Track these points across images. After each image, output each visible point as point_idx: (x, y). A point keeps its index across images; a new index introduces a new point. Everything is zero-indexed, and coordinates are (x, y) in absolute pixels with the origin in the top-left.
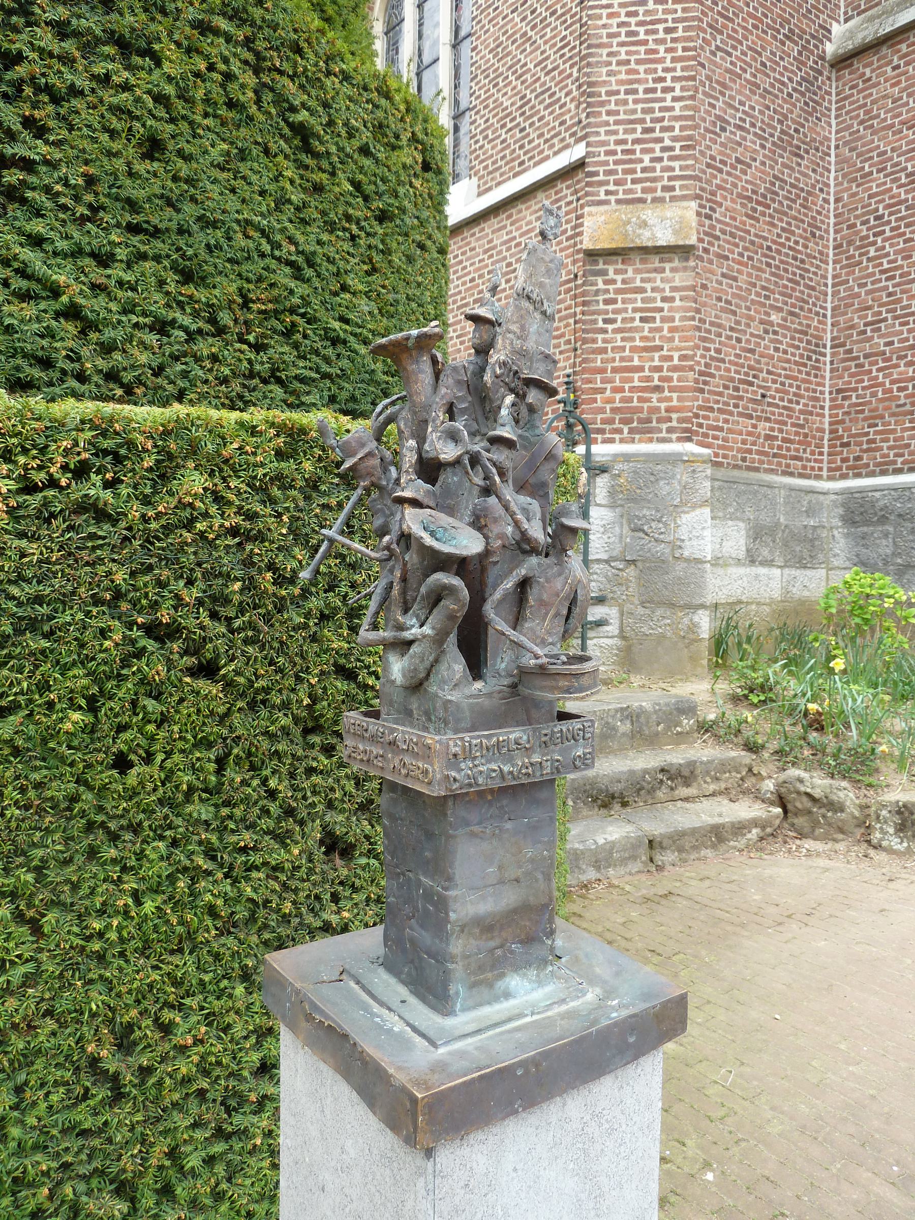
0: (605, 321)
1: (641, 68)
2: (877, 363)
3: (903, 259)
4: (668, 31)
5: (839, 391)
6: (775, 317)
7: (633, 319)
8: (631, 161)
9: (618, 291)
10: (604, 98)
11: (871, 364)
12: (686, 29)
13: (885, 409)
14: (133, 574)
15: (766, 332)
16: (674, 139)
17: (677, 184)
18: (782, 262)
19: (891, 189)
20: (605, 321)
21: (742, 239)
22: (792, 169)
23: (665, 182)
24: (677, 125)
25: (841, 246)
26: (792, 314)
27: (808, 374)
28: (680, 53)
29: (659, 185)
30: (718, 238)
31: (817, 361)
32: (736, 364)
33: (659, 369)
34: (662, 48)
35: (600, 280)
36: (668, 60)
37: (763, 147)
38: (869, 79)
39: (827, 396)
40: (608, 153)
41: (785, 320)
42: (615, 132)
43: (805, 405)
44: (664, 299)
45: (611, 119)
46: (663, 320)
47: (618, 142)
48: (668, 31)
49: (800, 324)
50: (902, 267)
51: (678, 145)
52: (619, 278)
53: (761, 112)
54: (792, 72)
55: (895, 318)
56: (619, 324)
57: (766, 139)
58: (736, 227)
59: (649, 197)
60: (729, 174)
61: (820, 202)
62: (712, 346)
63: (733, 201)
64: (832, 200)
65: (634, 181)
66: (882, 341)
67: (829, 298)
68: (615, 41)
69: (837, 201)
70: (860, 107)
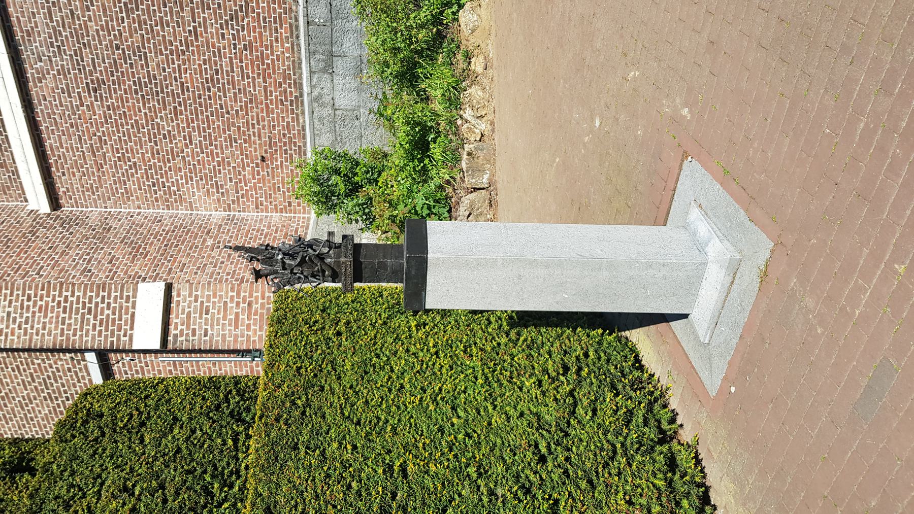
1: (50, 315)
4: (29, 299)
5: (257, 208)
6: (210, 242)
7: (206, 319)
8: (107, 322)
9: (188, 328)
10: (64, 338)
11: (242, 190)
12: (30, 289)
13: (269, 182)
16: (97, 296)
17: (125, 294)
18: (175, 239)
20: (206, 335)
22: (117, 233)
23: (123, 301)
24: (89, 294)
26: (208, 233)
27: (245, 225)
28: (44, 292)
29: (125, 304)
30: (158, 274)
31: (238, 219)
32: (237, 264)
33: (238, 304)
34: (39, 303)
35: (179, 339)
36: (47, 299)
37: (102, 249)
38: (67, 189)
40: (100, 336)
42: (88, 331)
43: (264, 226)
44: (196, 301)
45: (79, 333)
47: (94, 329)
48: (29, 299)
51: (101, 293)
52: (180, 327)
53: (80, 250)
54: (56, 232)
55: (216, 176)
56: (209, 327)
57: (98, 247)
59: (131, 310)
60: (118, 268)
63: (135, 265)
64: (138, 210)
65: (120, 319)
66: (229, 183)
67: (199, 212)
68: (29, 331)
69: (139, 208)
70: (84, 194)
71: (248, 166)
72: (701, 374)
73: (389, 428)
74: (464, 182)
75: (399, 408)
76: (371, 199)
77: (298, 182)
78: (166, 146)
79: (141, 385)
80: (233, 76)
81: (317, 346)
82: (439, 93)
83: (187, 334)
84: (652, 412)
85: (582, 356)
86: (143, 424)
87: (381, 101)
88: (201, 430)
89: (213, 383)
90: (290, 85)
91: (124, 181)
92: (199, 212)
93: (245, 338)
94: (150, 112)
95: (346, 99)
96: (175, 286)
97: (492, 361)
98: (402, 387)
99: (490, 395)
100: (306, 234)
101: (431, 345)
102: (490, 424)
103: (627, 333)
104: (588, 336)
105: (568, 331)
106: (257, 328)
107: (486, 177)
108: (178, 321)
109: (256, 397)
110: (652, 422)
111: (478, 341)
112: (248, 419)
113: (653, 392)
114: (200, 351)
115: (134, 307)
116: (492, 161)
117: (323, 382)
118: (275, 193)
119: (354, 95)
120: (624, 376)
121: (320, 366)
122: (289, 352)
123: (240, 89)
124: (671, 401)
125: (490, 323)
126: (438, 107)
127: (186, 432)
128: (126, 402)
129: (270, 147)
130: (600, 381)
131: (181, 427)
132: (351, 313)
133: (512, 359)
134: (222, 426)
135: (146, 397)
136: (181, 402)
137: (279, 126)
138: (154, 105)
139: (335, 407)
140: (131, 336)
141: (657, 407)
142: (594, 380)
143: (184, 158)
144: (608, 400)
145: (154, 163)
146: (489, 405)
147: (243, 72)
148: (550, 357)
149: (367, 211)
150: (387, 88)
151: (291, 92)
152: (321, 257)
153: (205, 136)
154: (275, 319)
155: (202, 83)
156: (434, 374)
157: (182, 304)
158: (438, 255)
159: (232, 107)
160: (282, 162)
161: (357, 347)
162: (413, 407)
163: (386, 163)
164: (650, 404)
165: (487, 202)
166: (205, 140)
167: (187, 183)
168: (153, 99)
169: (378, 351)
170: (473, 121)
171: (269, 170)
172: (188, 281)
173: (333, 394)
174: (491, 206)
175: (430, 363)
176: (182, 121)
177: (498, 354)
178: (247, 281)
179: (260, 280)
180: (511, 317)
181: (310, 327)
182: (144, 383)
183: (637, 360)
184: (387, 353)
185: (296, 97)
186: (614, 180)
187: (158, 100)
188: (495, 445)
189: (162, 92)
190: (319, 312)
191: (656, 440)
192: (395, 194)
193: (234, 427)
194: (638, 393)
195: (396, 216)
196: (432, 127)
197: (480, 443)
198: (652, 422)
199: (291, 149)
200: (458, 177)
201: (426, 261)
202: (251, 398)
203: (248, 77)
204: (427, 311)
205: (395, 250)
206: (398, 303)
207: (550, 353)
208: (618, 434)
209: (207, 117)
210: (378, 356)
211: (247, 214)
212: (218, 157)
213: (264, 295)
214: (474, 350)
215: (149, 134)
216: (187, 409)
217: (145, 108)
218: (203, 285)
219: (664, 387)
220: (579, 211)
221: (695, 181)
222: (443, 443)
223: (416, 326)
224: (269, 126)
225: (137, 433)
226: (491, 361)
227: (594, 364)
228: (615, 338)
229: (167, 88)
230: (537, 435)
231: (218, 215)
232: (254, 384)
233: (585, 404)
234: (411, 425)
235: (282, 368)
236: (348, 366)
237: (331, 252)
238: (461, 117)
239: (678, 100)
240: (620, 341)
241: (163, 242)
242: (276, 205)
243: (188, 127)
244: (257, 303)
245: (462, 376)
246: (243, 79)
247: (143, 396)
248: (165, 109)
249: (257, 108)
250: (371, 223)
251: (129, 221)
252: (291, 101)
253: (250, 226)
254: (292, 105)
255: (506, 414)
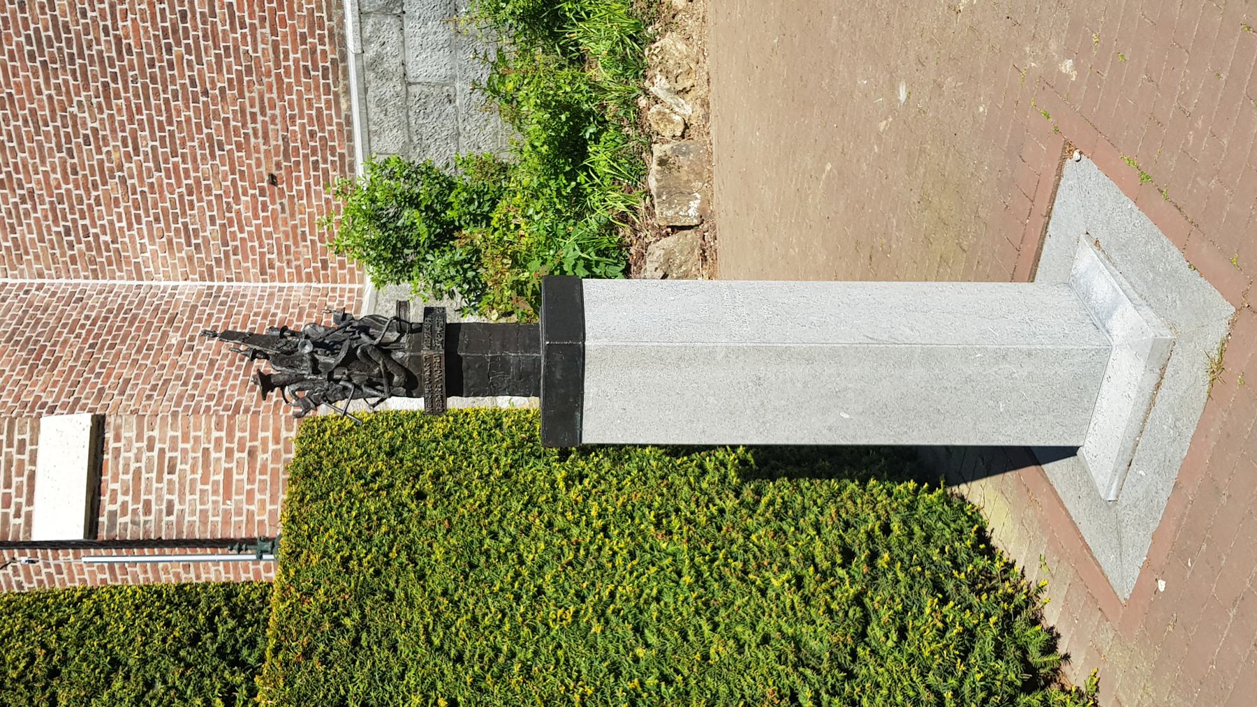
0: (169, 513)
2: (233, 233)
3: (117, 206)
5: (263, 272)
6: (174, 339)
7: (170, 482)
9: (136, 499)
14: (498, 468)
15: (191, 348)
17: (17, 437)
18: (109, 333)
19: (37, 219)
20: (169, 513)
21: (80, 374)
23: (14, 450)
25: (94, 271)
26: (171, 321)
27: (241, 305)
29: (16, 457)
30: (78, 399)
31: (227, 295)
32: (227, 379)
33: (229, 453)
35: (120, 520)
39: (268, 284)
41: (178, 328)
43: (277, 307)
44: (150, 448)
46: (173, 448)
49: (183, 313)
50: (127, 208)
52: (121, 498)
55: (184, 214)
56: (175, 498)
58: (66, 381)
59: (28, 468)
61: (41, 293)
62: (204, 404)
63: (34, 384)
66: (209, 228)
67: (154, 283)
69: (41, 275)
71: (245, 194)
72: (1101, 560)
73: (516, 668)
74: (652, 215)
75: (534, 630)
76: (477, 251)
77: (340, 222)
78: (90, 158)
79: (50, 601)
80: (214, 24)
81: (380, 519)
82: (603, 48)
83: (135, 511)
84: (1010, 633)
85: (878, 532)
86: (54, 673)
87: (495, 66)
88: (165, 682)
89: (185, 596)
90: (321, 38)
91: (12, 226)
92: (154, 283)
93: (244, 518)
94: (59, 94)
95: (427, 65)
96: (110, 420)
97: (710, 541)
98: (540, 591)
99: (706, 604)
100: (360, 303)
101: (594, 513)
102: (706, 657)
103: (963, 489)
104: (890, 494)
105: (853, 486)
106: (267, 497)
107: (695, 204)
108: (117, 486)
109: (267, 620)
110: (1011, 652)
111: (682, 505)
112: (251, 660)
113: (1011, 597)
114: (159, 543)
115: (33, 461)
116: (705, 175)
117: (392, 584)
118: (296, 244)
119: (443, 57)
120: (957, 566)
121: (386, 555)
122: (327, 530)
123: (227, 48)
124: (1047, 612)
125: (704, 472)
126: (601, 74)
127: (135, 686)
128: (22, 632)
129: (287, 158)
130: (913, 577)
131: (127, 678)
132: (442, 458)
133: (747, 538)
134: (203, 675)
135: (60, 623)
136: (126, 632)
137: (301, 117)
138: (66, 82)
139: (416, 631)
140: (29, 516)
141: (1019, 623)
142: (901, 575)
143: (123, 181)
144: (928, 611)
145: (68, 191)
146: (703, 622)
147: (232, 15)
148: (819, 533)
149: (470, 274)
150: (506, 40)
151: (324, 52)
152: (385, 350)
153: (163, 139)
154: (300, 470)
155: (156, 37)
156: (600, 566)
157: (123, 454)
158: (604, 342)
159: (212, 81)
160: (308, 186)
161: (455, 520)
162: (562, 629)
163: (504, 184)
164: (1008, 619)
165: (697, 252)
166: (163, 145)
167: (130, 227)
168: (64, 68)
169: (495, 527)
170: (669, 99)
171: (285, 201)
172: (135, 412)
173: (411, 605)
174: (704, 259)
175: (593, 548)
176: (119, 110)
177: (719, 529)
178: (247, 411)
179: (274, 395)
180: (744, 462)
181: (366, 484)
182: (56, 597)
183: (982, 536)
184: (512, 529)
185: (333, 61)
186: (935, 201)
187: (74, 72)
188: (715, 696)
189: (81, 55)
190: (382, 456)
191: (1019, 683)
192: (524, 241)
193: (227, 674)
194: (984, 596)
195: (526, 283)
196: (590, 113)
197: (687, 693)
198: (1011, 652)
199: (325, 161)
200: (641, 207)
201: (581, 353)
202: (257, 621)
203: (243, 26)
204: (586, 451)
205: (523, 335)
206: (531, 439)
207: (817, 527)
208: (947, 672)
209: (167, 101)
210: (494, 536)
211: (243, 284)
212: (187, 177)
213: (277, 428)
214: (676, 523)
215: (57, 135)
216: (137, 644)
217: (48, 88)
218: (164, 419)
219: (1033, 586)
220: (871, 261)
221: (1087, 196)
222: (619, 694)
223: (566, 479)
224: (284, 118)
225: (44, 689)
226: (707, 541)
227: (901, 545)
228: (939, 497)
229: (90, 47)
230: (794, 677)
231: (189, 288)
232: (263, 597)
233: (885, 618)
234: (558, 661)
235: (315, 559)
236: (439, 554)
237: (404, 340)
238: (646, 92)
239: (1053, 46)
240: (949, 503)
241: (86, 340)
242: (298, 267)
243: (131, 121)
244: (265, 451)
245: (653, 570)
246: (233, 30)
247: (53, 621)
248: (87, 88)
249: (260, 82)
250: (479, 298)
251: (22, 300)
252: (325, 69)
253: (250, 307)
254: (325, 77)
255: (737, 640)
